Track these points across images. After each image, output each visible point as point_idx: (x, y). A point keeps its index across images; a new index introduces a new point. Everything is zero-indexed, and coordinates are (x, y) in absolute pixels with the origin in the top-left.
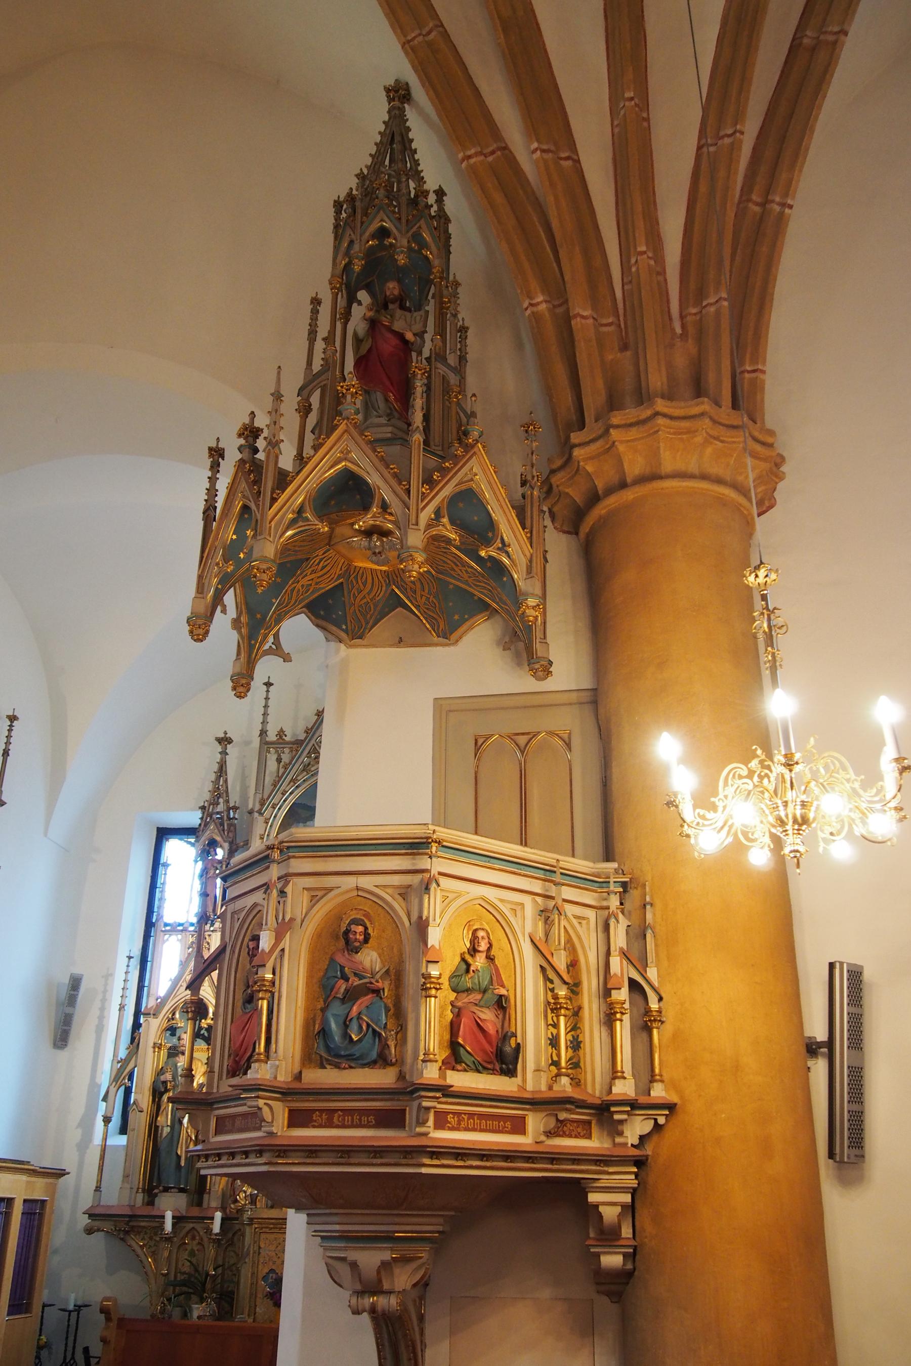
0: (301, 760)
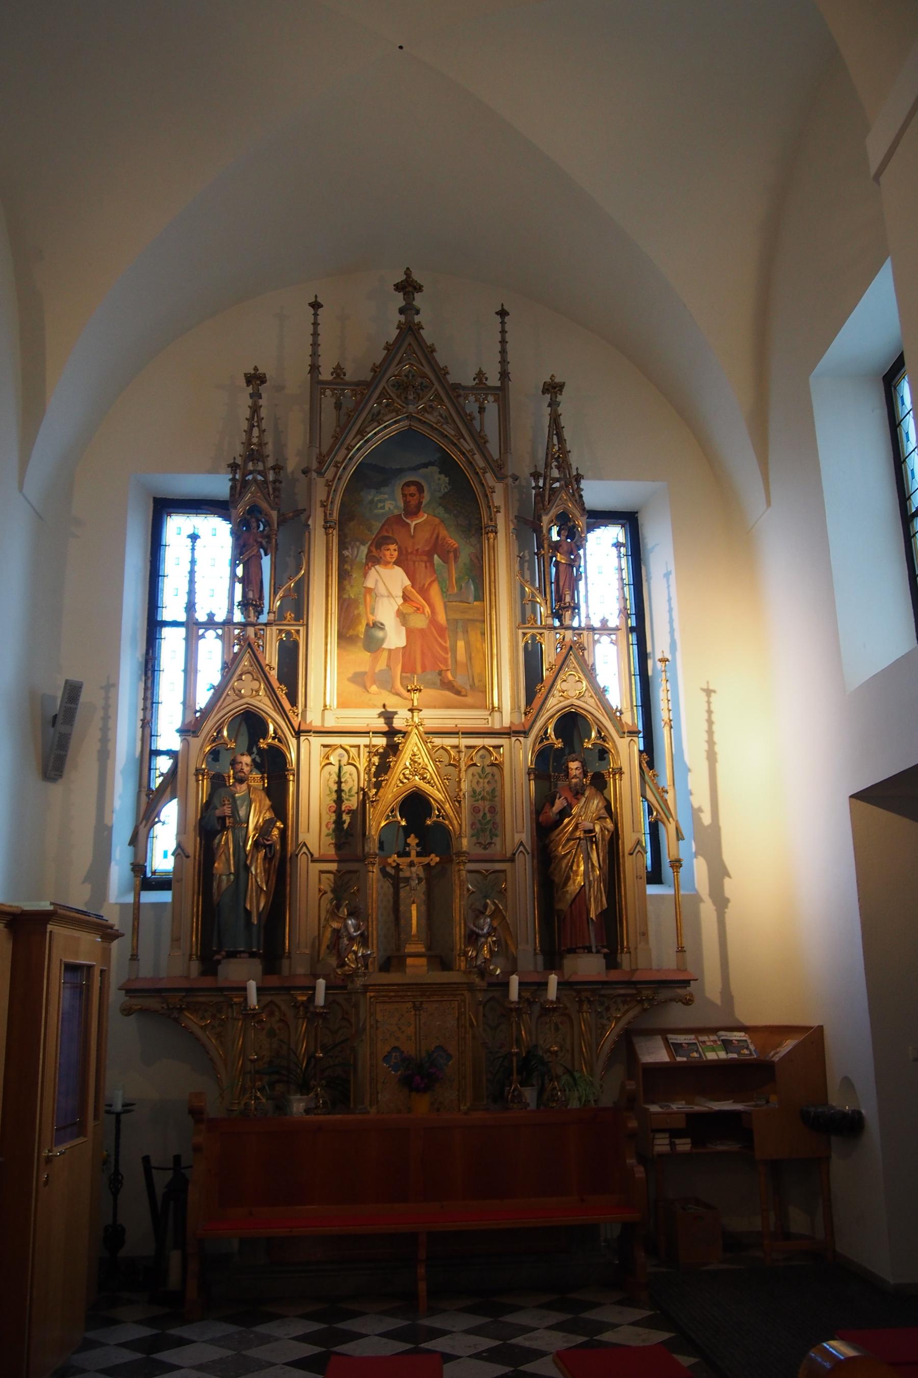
0: (369, 406)
